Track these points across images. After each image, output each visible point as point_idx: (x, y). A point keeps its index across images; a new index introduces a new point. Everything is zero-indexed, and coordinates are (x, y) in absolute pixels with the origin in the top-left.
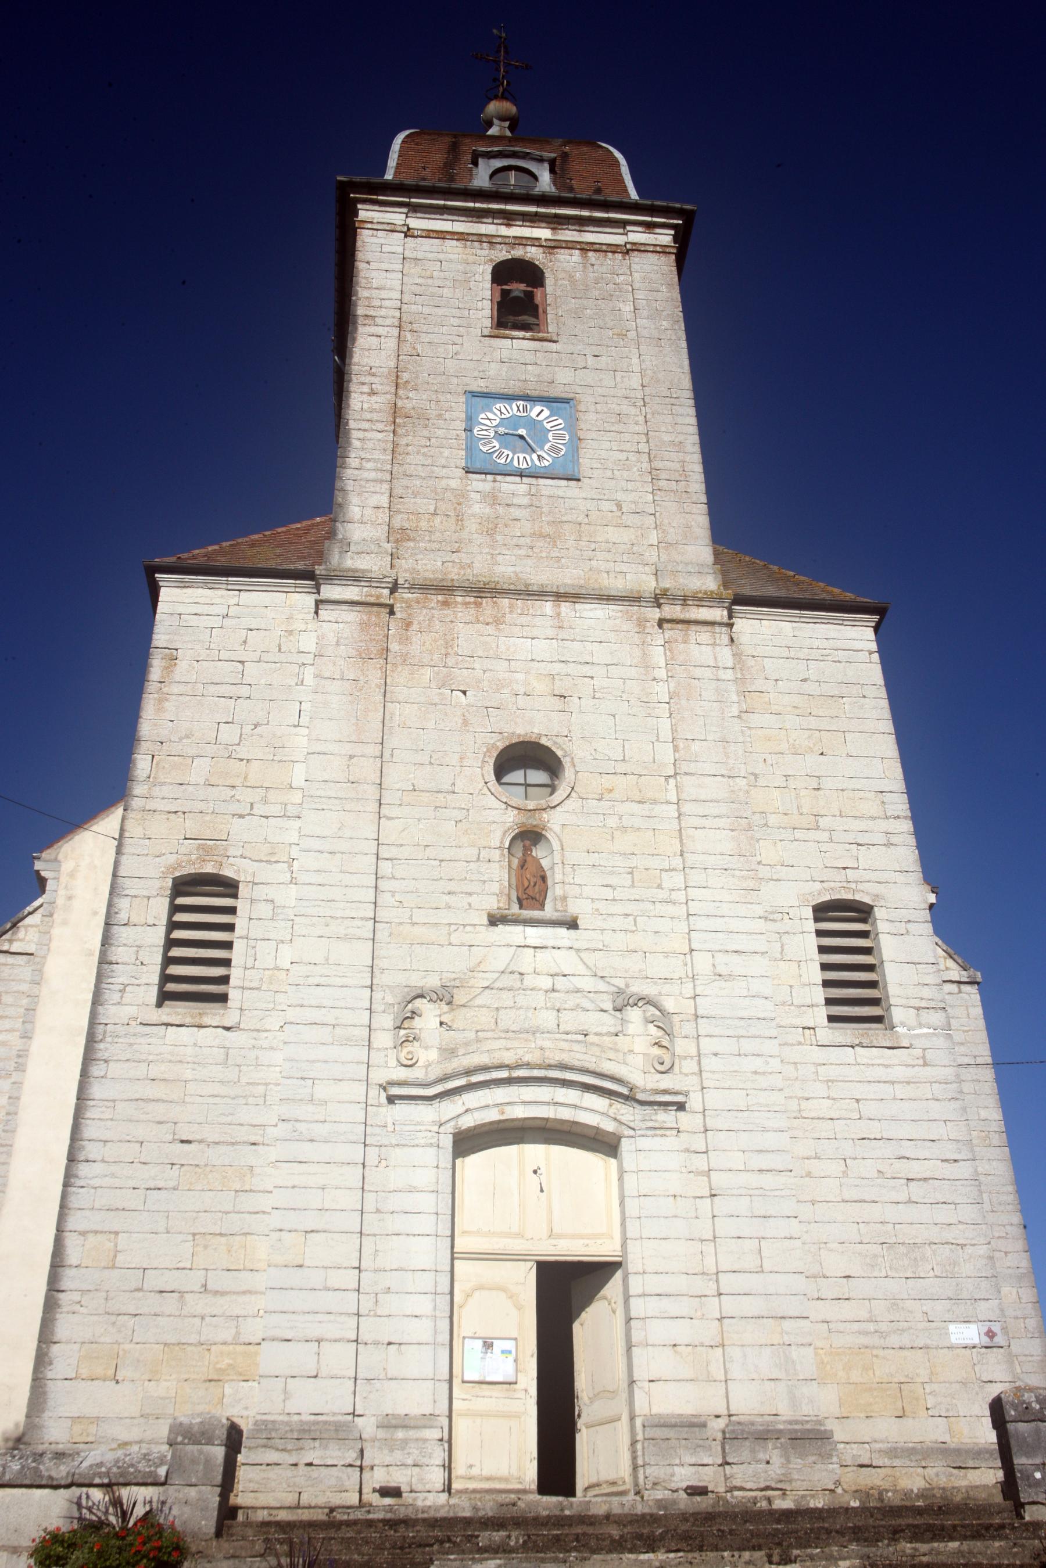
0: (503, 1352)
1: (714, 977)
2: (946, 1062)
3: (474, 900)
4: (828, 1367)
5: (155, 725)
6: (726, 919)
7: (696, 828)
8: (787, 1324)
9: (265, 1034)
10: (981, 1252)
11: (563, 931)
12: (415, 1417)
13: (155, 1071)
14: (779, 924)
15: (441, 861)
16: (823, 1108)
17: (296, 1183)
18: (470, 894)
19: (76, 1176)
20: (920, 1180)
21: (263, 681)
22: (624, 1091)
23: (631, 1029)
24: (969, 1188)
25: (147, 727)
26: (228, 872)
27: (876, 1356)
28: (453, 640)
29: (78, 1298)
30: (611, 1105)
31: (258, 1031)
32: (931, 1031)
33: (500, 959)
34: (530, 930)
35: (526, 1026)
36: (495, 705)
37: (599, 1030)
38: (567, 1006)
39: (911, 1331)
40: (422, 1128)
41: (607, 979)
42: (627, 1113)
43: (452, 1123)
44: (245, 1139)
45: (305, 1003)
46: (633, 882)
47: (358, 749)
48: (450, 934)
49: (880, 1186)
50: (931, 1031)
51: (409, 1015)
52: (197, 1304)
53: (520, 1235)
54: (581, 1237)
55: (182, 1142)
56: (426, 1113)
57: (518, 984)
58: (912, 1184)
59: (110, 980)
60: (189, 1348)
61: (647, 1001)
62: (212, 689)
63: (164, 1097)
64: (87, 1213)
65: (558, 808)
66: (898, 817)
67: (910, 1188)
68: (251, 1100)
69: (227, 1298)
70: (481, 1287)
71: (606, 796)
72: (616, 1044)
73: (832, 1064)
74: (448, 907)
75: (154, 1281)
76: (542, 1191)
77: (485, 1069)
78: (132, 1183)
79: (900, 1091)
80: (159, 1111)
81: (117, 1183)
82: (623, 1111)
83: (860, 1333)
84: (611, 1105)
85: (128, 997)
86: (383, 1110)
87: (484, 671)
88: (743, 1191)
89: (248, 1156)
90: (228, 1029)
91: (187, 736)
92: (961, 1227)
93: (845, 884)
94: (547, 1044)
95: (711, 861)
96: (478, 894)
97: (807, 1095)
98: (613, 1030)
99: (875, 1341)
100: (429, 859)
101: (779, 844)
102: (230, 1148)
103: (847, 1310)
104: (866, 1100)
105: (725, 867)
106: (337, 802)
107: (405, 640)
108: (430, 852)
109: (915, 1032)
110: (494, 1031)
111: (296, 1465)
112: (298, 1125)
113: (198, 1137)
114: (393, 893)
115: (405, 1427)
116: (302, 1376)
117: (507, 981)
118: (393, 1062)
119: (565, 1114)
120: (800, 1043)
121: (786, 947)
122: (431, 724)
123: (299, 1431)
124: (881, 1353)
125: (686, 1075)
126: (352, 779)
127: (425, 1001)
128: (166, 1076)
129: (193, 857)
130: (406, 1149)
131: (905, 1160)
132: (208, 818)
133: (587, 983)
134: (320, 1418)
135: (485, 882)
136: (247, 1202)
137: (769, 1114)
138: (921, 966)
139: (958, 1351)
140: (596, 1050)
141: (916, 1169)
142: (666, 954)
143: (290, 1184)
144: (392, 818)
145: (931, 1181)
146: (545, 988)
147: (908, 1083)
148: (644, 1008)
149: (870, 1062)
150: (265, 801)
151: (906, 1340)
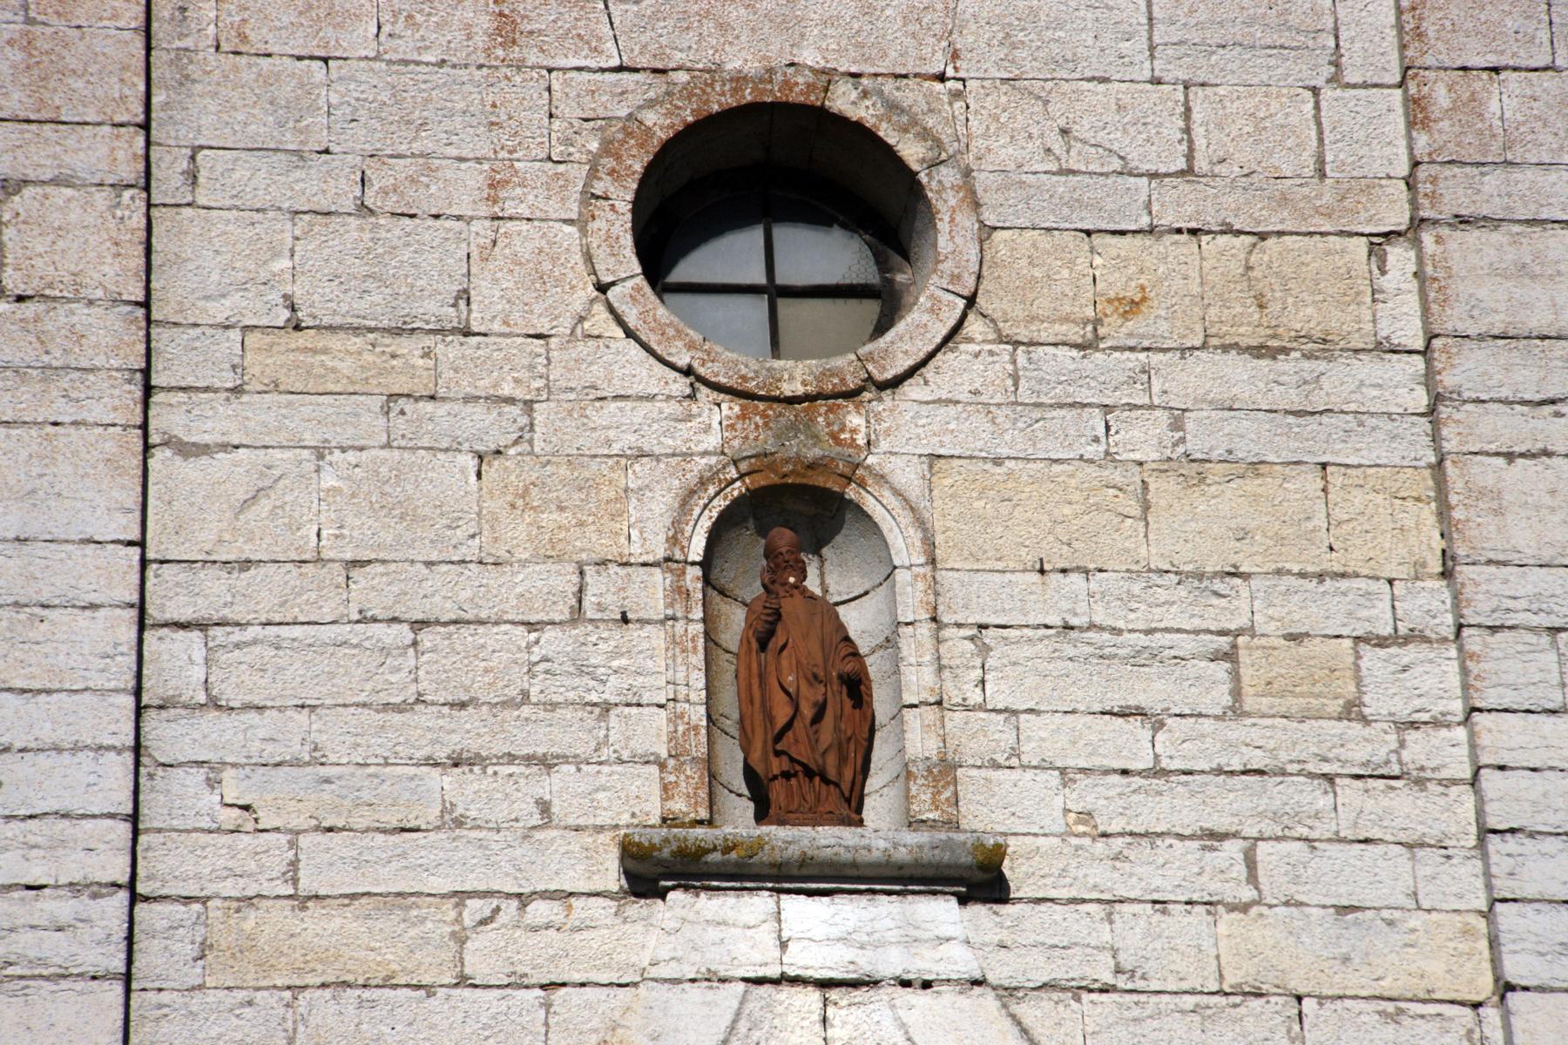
7: (1510, 457)
11: (940, 912)
15: (419, 625)
18: (546, 763)
34: (802, 911)
46: (1237, 693)
48: (460, 939)
71: (1116, 330)
108: (370, 590)
114: (213, 772)
135: (606, 708)
144: (203, 450)
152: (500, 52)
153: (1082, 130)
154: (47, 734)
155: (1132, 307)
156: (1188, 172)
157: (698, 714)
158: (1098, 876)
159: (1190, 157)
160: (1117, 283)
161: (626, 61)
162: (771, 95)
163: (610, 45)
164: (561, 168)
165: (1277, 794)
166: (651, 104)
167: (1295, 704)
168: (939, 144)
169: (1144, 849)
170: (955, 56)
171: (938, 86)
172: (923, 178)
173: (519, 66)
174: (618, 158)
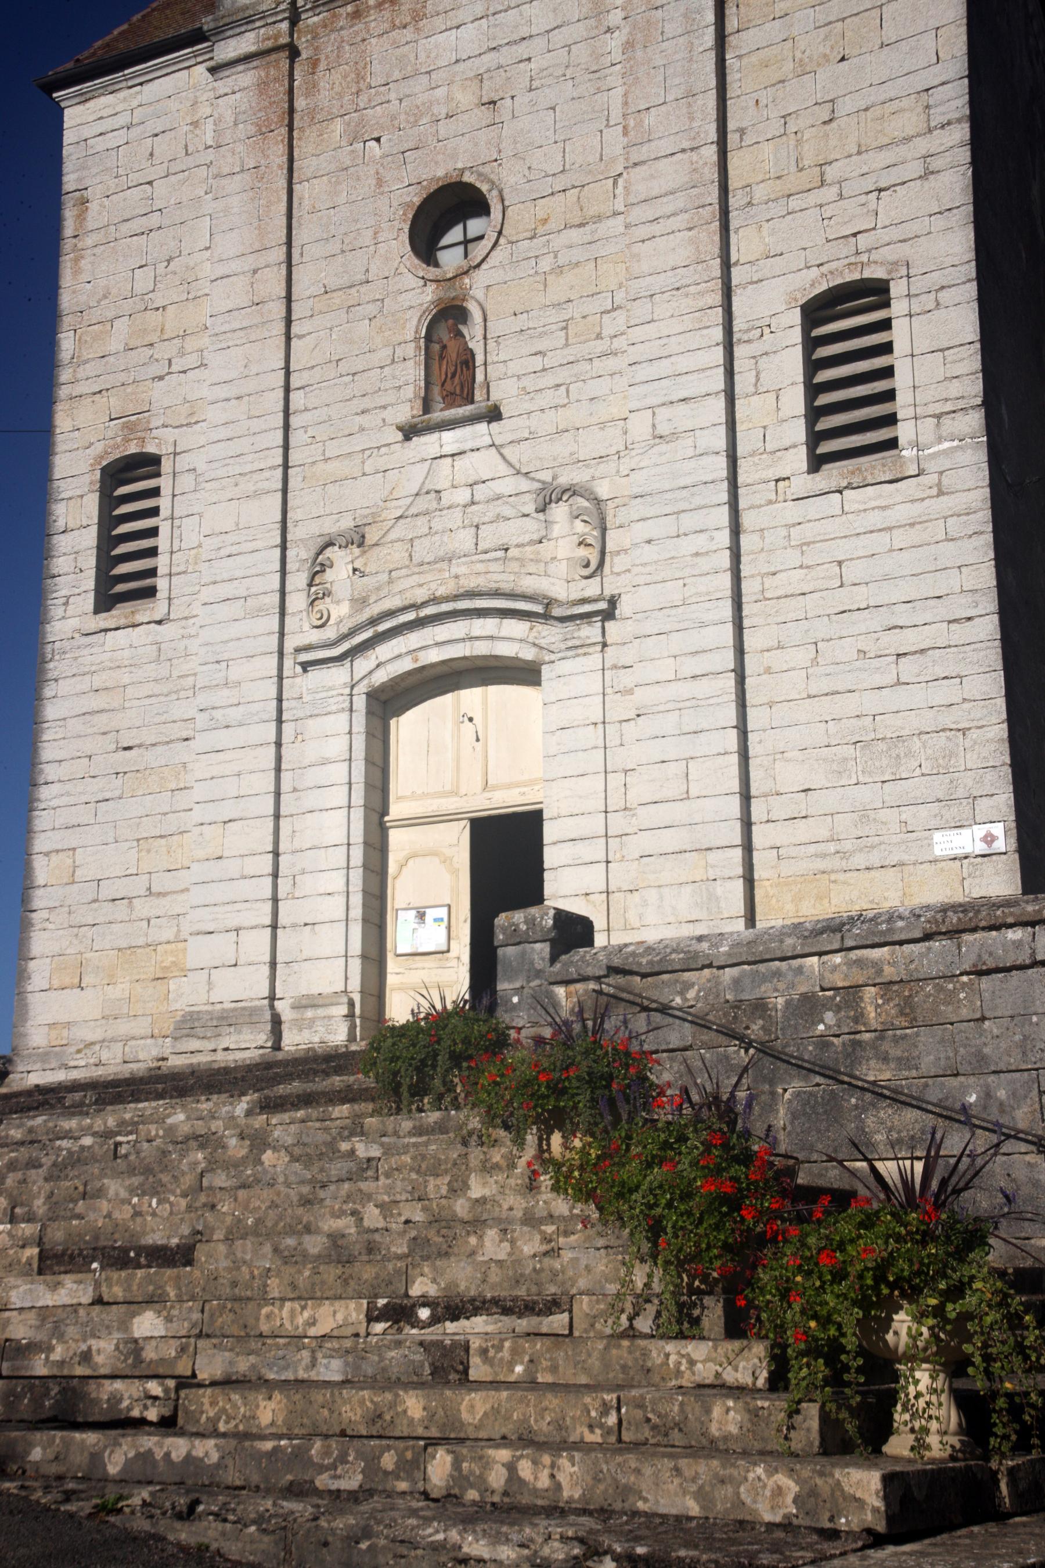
0: (435, 920)
1: (652, 442)
2: (971, 484)
3: (388, 414)
4: (774, 900)
5: (74, 292)
6: (673, 359)
7: (643, 241)
8: (712, 856)
9: (192, 621)
10: (990, 735)
11: (482, 427)
12: (328, 996)
13: (98, 681)
14: (755, 345)
15: (354, 374)
16: (794, 580)
17: (214, 774)
18: (384, 407)
19: (39, 800)
20: (916, 652)
21: (172, 202)
22: (539, 609)
23: (557, 530)
24: (982, 653)
25: (67, 300)
26: (151, 449)
27: (835, 882)
28: (365, 68)
29: (46, 916)
30: (531, 629)
31: (186, 618)
32: (956, 443)
33: (414, 478)
34: (447, 436)
35: (441, 553)
36: (411, 145)
37: (520, 540)
38: (486, 519)
39: (883, 847)
40: (334, 693)
41: (532, 475)
42: (550, 634)
43: (365, 682)
44: (178, 736)
45: (218, 579)
46: (567, 339)
47: (261, 260)
48: (363, 463)
49: (860, 669)
50: (956, 443)
51: (318, 569)
52: (143, 908)
53: (455, 793)
54: (518, 785)
55: (126, 749)
56: (338, 676)
57: (434, 505)
58: (902, 660)
59: (54, 595)
60: (139, 951)
61: (572, 491)
62: (125, 228)
63: (107, 706)
64: (49, 834)
65: (484, 266)
66: (949, 123)
67: (900, 665)
68: (182, 694)
69: (169, 898)
70: (414, 856)
71: (540, 230)
72: (538, 553)
73: (809, 521)
74: (362, 429)
75: (108, 891)
76: (478, 740)
77: (390, 614)
78: (84, 799)
79: (900, 538)
80: (102, 721)
81: (72, 800)
82: (545, 633)
83: (816, 856)
84: (531, 629)
85: (71, 610)
86: (298, 680)
87: (401, 100)
88: (670, 706)
89: (181, 753)
90: (159, 622)
91: (105, 297)
92: (966, 705)
93: (853, 259)
94: (462, 570)
95: (657, 283)
96: (392, 405)
97: (773, 569)
98: (536, 537)
99: (836, 863)
100: (341, 376)
101: (765, 225)
102: (166, 747)
103: (803, 831)
104: (852, 559)
105: (677, 285)
106: (241, 333)
107: (312, 88)
108: (343, 367)
109: (931, 451)
110: (407, 567)
111: (215, 1051)
112: (214, 713)
113: (138, 742)
114: (305, 428)
115: (314, 1006)
116: (223, 966)
117: (425, 503)
118: (306, 627)
119: (481, 649)
120: (770, 502)
121: (762, 375)
122: (342, 199)
123: (219, 1019)
124: (841, 877)
125: (618, 574)
126: (256, 301)
127: (336, 548)
128: (108, 684)
129: (119, 439)
130: (319, 719)
131: (897, 631)
132: (129, 390)
133: (507, 485)
134: (240, 1005)
135: (400, 387)
136: (183, 800)
137: (708, 605)
138: (952, 351)
139: (943, 864)
140: (514, 566)
141: (910, 640)
142: (602, 425)
143: (209, 776)
144: (303, 336)
145: (930, 652)
146: (462, 503)
147: (912, 525)
148: (571, 501)
149: (862, 507)
150: (182, 353)
151: (875, 859)
154: (264, 427)
155: (545, 221)
157: (422, 384)
158: (527, 406)
160: (541, 214)
165: (575, 368)
167: (583, 338)
169: (539, 395)
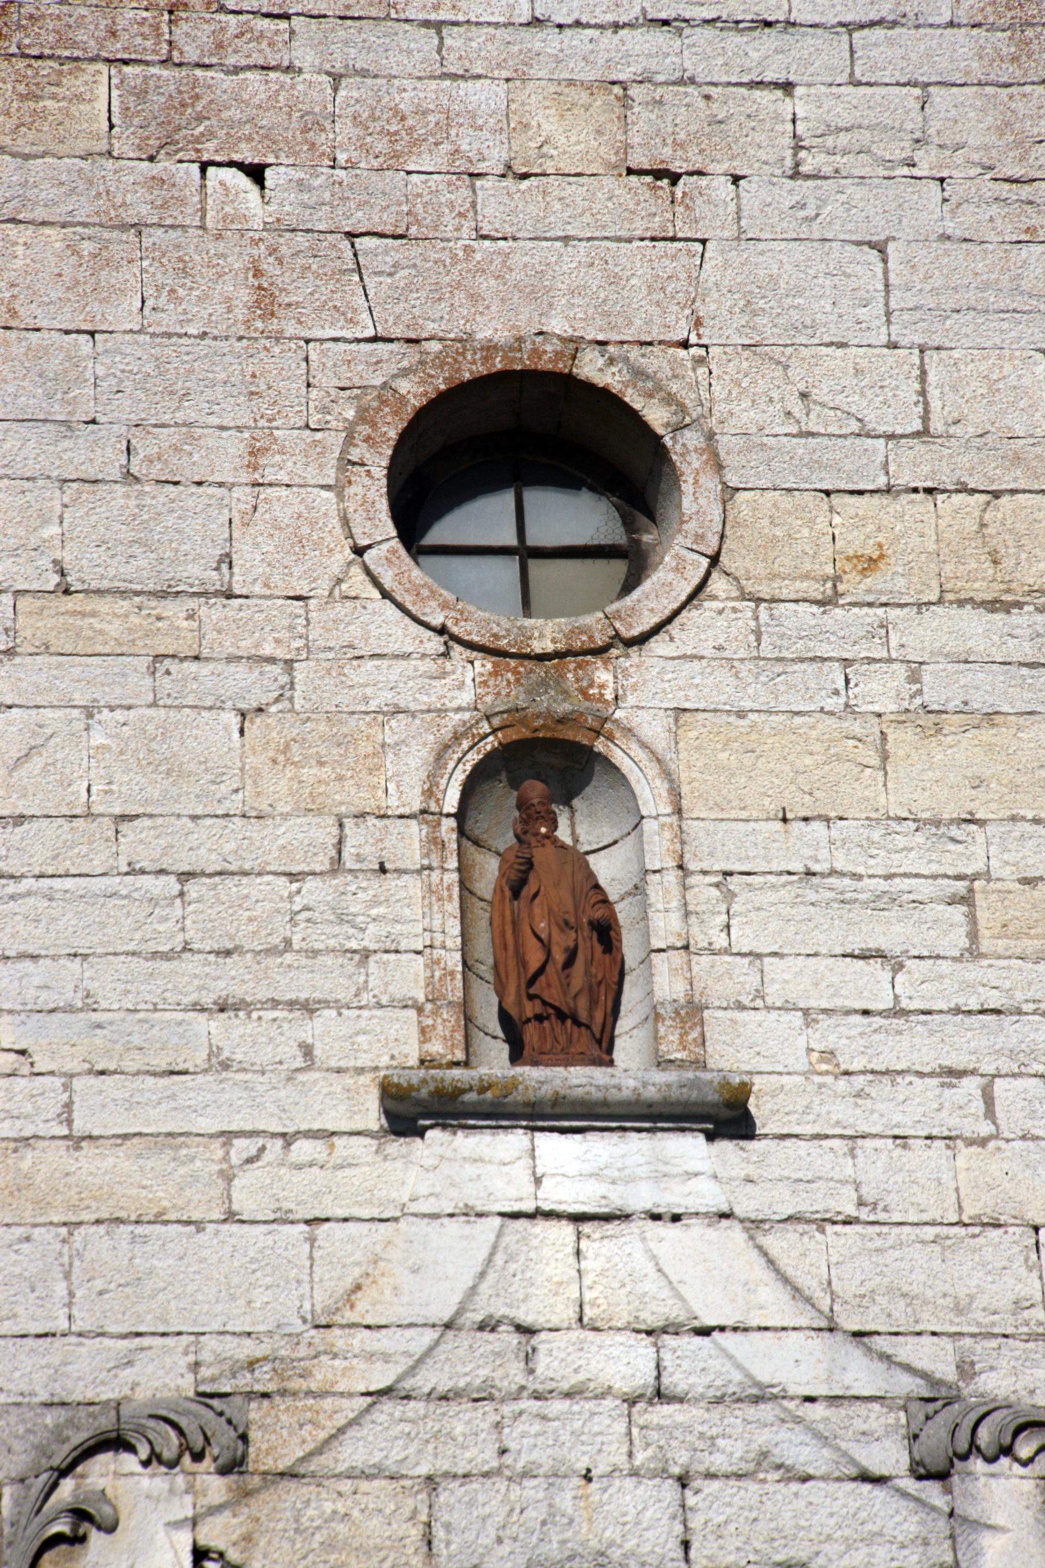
152: (259, 324)
153: (820, 393)
156: (924, 433)
159: (925, 418)
161: (381, 332)
162: (523, 362)
163: (365, 316)
164: (319, 436)
166: (404, 373)
168: (683, 408)
170: (698, 323)
171: (682, 353)
172: (668, 441)
173: (278, 337)
174: (374, 425)
